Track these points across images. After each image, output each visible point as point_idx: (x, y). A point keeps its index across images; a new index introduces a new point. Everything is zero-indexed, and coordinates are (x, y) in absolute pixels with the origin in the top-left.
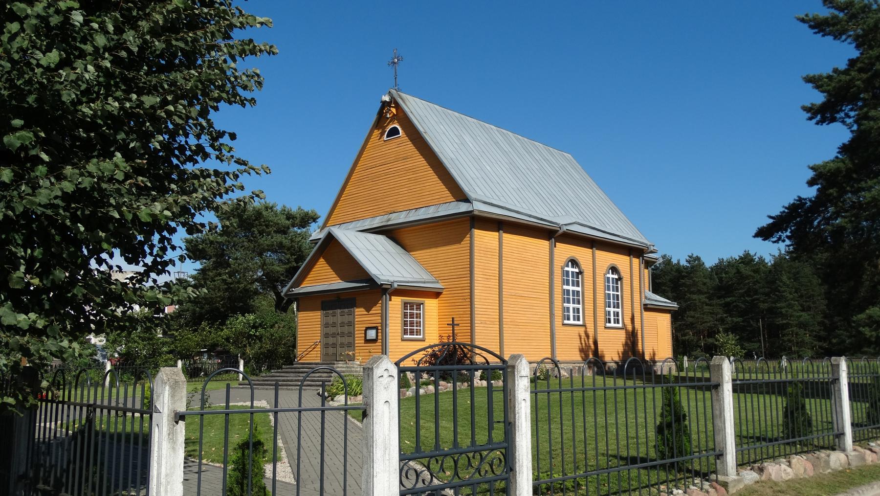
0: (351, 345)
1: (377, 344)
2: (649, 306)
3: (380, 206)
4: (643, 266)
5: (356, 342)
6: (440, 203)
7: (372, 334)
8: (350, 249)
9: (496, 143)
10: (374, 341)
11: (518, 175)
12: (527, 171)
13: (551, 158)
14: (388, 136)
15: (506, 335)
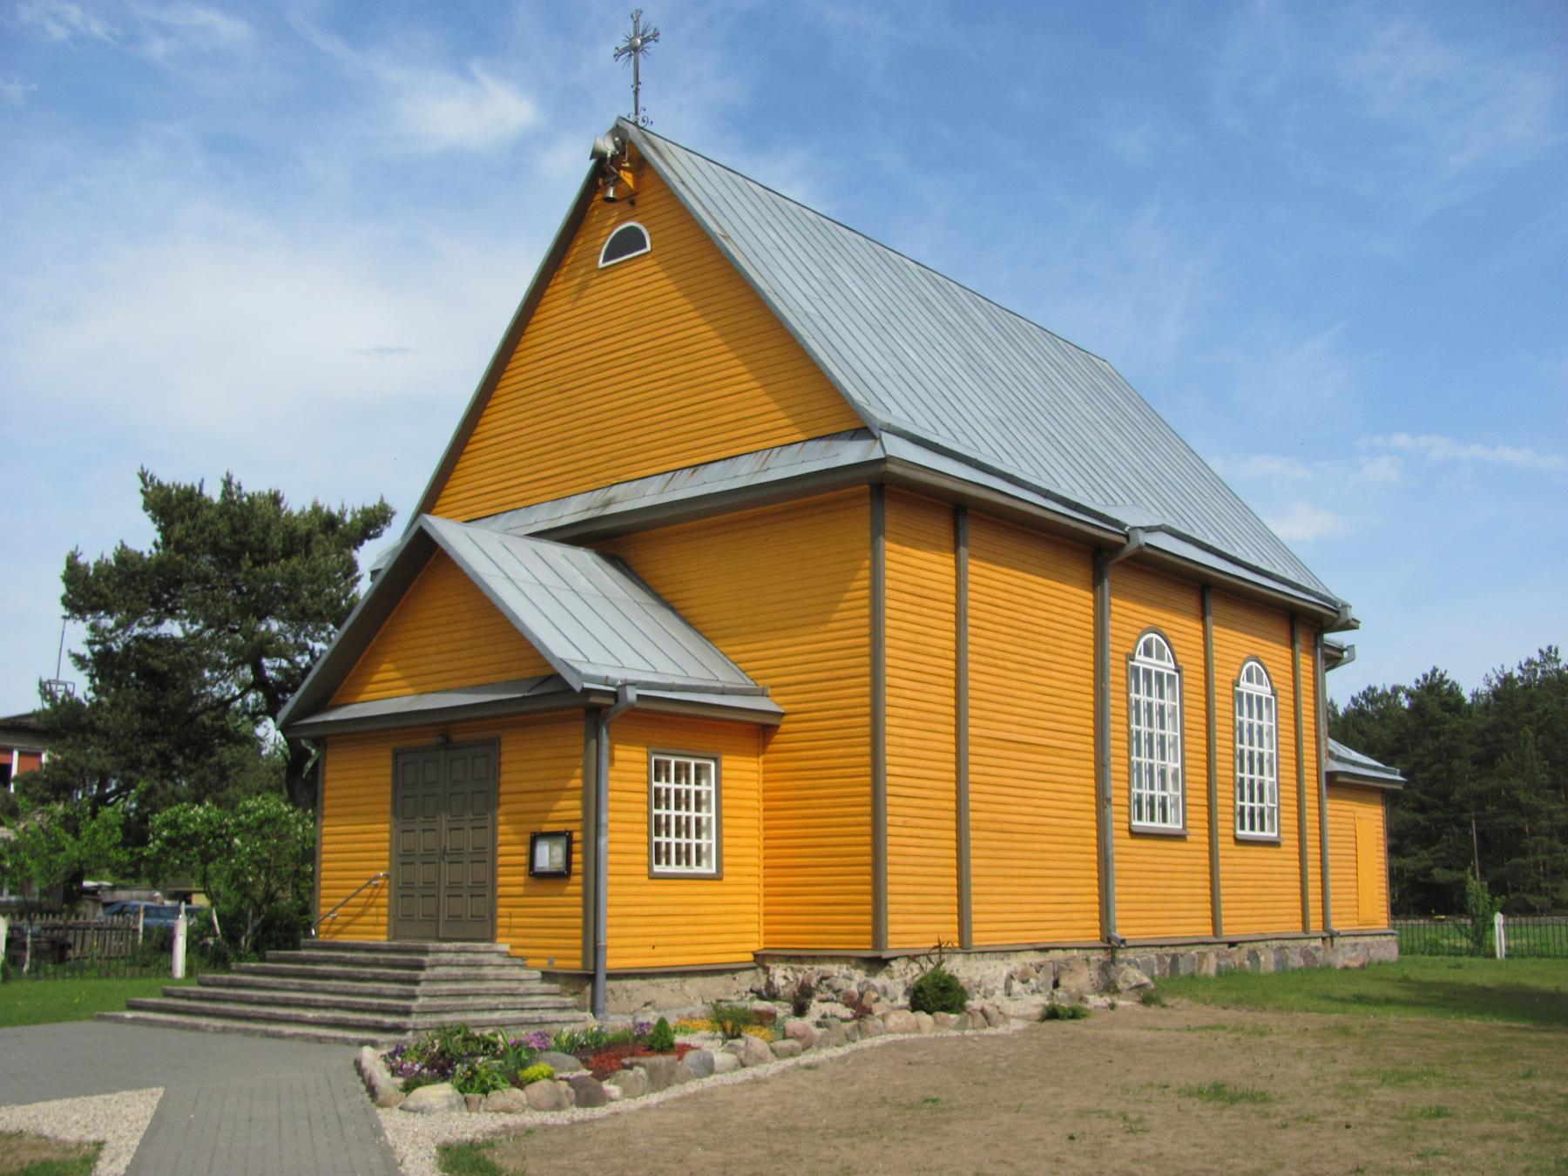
0: (485, 889)
1: (570, 889)
2: (1340, 779)
3: (583, 464)
4: (1321, 664)
5: (501, 880)
6: (771, 444)
7: (548, 856)
8: (483, 577)
9: (925, 301)
10: (560, 876)
11: (994, 387)
12: (1014, 380)
13: (1065, 361)
14: (605, 260)
15: (976, 864)
